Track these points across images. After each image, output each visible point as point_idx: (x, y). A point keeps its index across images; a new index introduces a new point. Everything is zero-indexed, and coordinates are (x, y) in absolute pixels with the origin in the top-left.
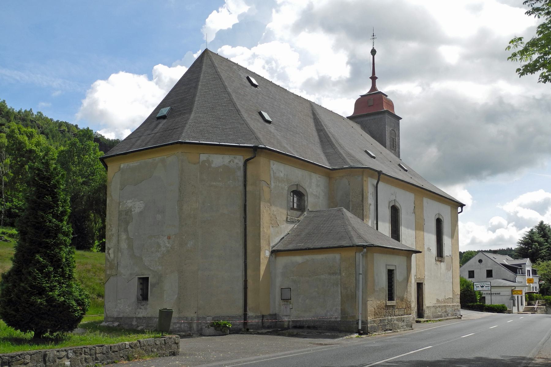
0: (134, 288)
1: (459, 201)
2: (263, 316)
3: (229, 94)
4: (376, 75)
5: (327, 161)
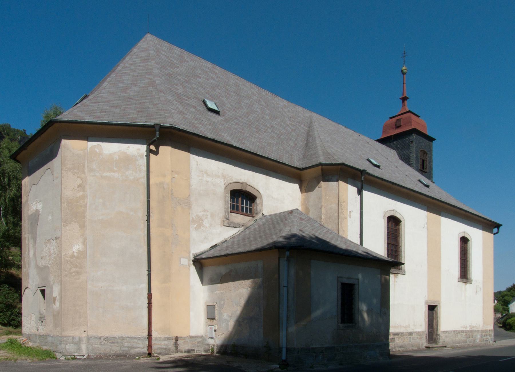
1: (473, 267)
2: (177, 339)
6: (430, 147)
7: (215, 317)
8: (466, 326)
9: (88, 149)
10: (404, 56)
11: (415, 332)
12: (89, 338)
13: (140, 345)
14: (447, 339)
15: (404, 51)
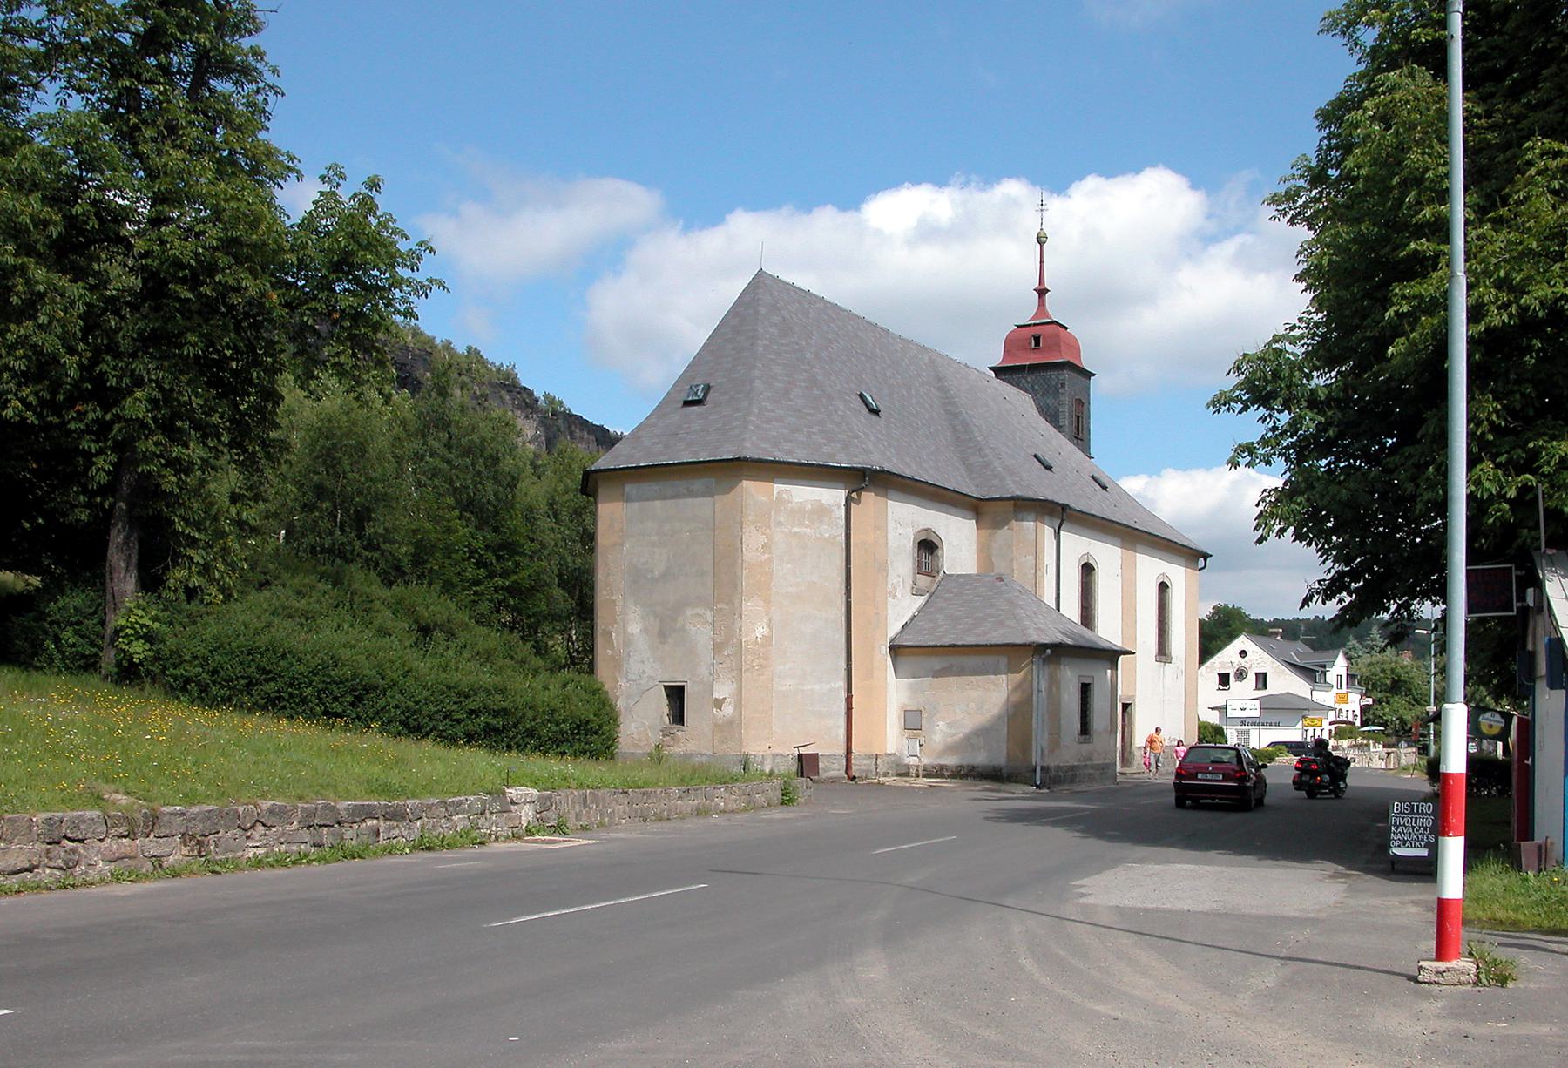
13: (836, 766)
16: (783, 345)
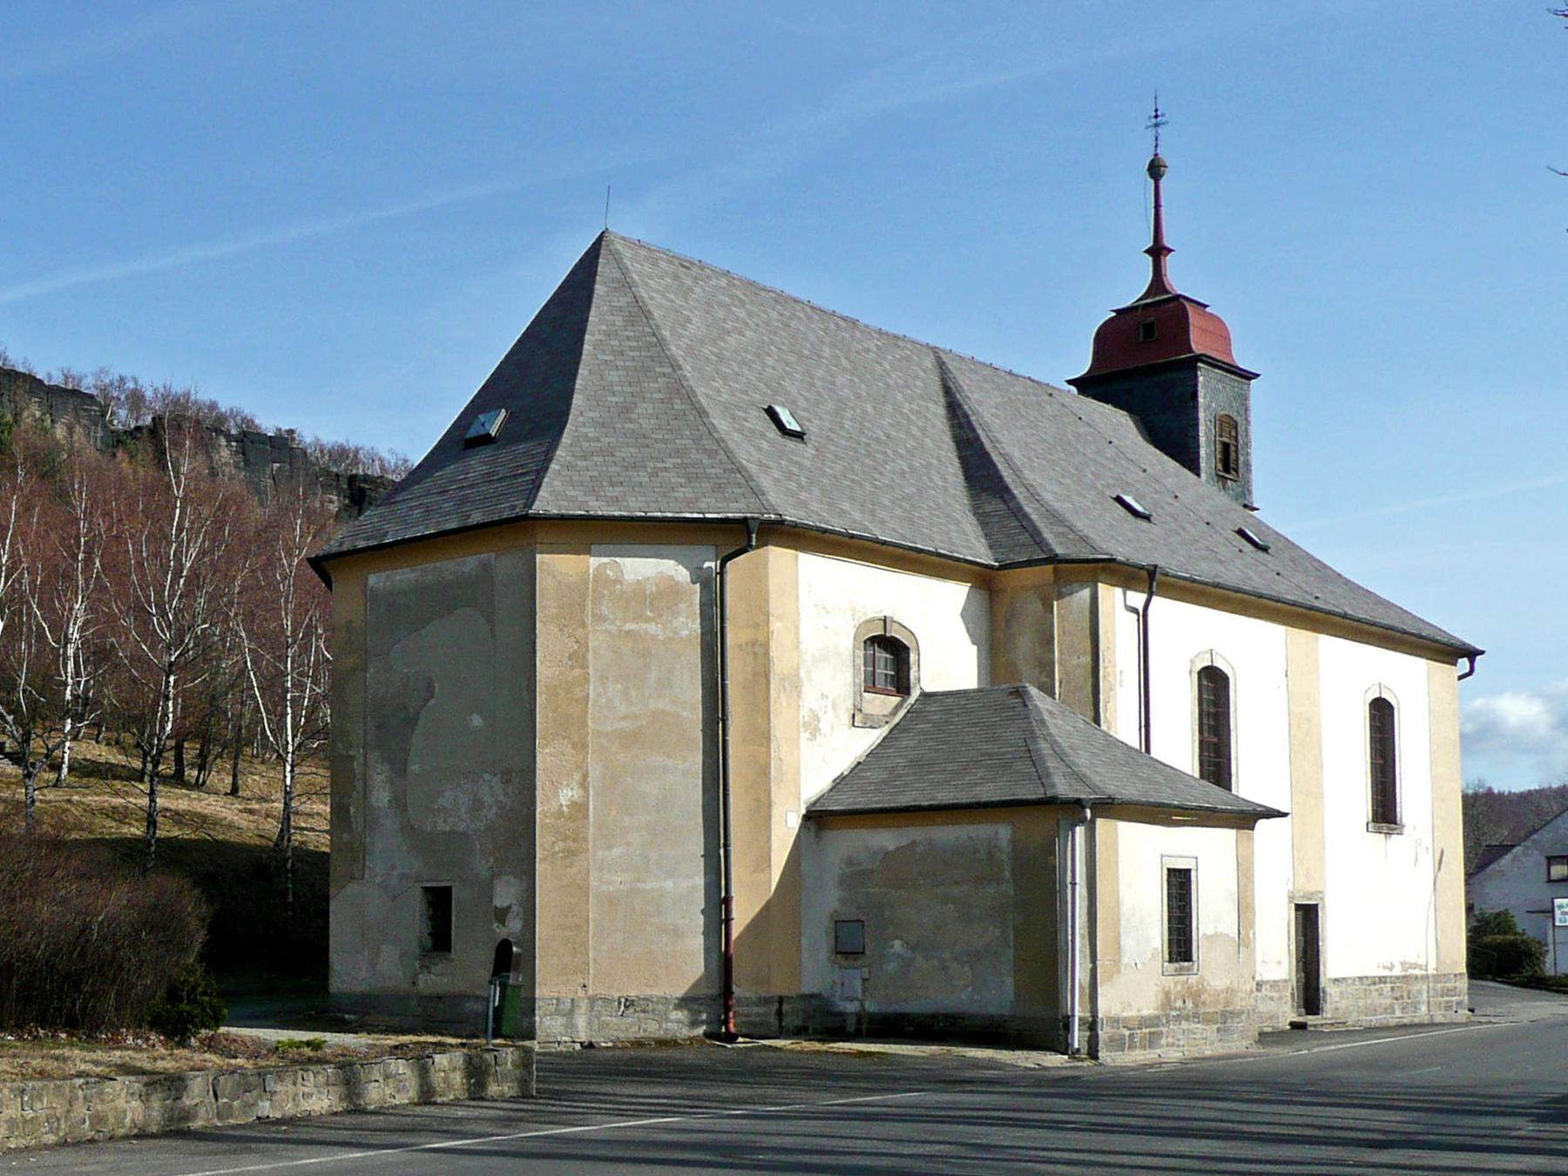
0: (414, 920)
2: (781, 1000)
3: (675, 366)
4: (1167, 241)
5: (983, 540)
6: (1244, 399)
7: (864, 948)
8: (1392, 964)
9: (591, 571)
10: (1157, 125)
11: (1267, 982)
12: (593, 1000)
14: (1344, 1002)
15: (1156, 110)
16: (628, 338)
